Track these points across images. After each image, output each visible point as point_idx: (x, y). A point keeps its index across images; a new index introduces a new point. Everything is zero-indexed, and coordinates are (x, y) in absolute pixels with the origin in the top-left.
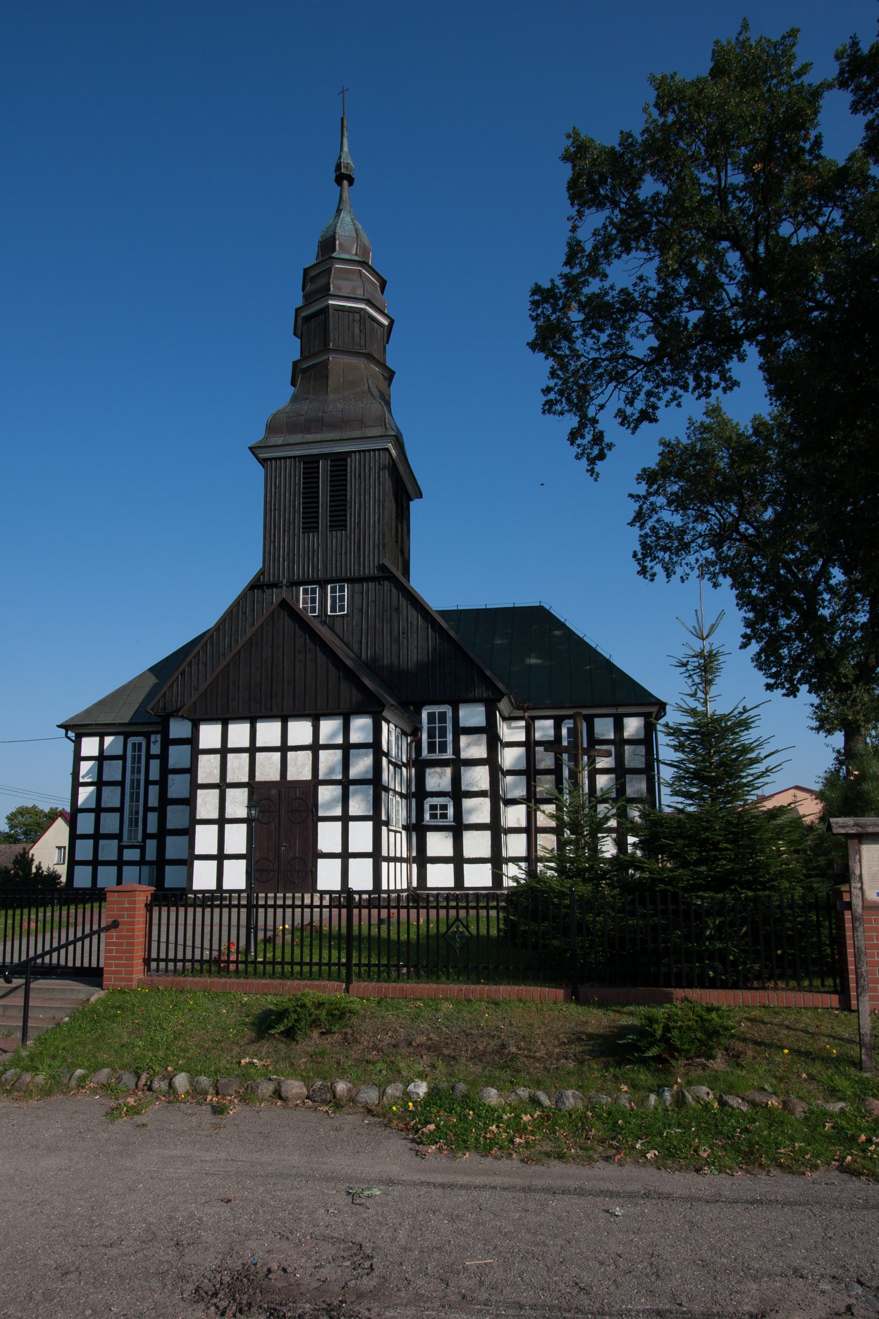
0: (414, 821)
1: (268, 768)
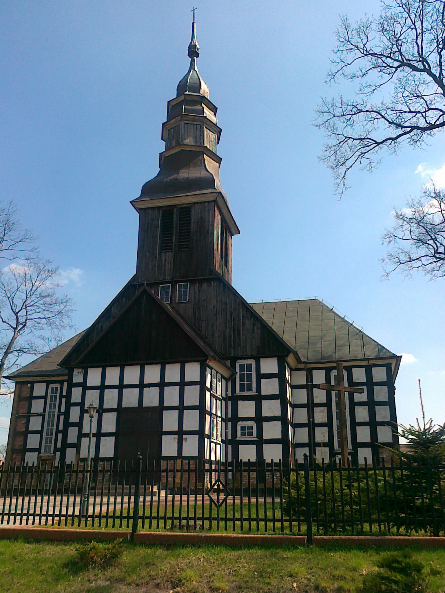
0: (230, 437)
1: (131, 398)
